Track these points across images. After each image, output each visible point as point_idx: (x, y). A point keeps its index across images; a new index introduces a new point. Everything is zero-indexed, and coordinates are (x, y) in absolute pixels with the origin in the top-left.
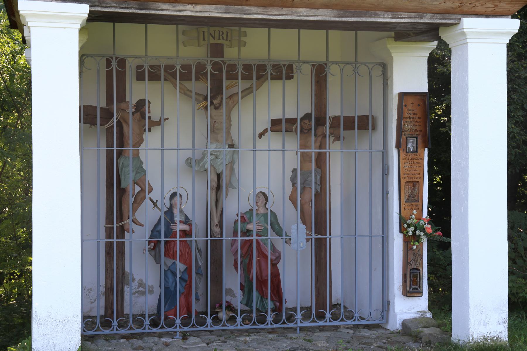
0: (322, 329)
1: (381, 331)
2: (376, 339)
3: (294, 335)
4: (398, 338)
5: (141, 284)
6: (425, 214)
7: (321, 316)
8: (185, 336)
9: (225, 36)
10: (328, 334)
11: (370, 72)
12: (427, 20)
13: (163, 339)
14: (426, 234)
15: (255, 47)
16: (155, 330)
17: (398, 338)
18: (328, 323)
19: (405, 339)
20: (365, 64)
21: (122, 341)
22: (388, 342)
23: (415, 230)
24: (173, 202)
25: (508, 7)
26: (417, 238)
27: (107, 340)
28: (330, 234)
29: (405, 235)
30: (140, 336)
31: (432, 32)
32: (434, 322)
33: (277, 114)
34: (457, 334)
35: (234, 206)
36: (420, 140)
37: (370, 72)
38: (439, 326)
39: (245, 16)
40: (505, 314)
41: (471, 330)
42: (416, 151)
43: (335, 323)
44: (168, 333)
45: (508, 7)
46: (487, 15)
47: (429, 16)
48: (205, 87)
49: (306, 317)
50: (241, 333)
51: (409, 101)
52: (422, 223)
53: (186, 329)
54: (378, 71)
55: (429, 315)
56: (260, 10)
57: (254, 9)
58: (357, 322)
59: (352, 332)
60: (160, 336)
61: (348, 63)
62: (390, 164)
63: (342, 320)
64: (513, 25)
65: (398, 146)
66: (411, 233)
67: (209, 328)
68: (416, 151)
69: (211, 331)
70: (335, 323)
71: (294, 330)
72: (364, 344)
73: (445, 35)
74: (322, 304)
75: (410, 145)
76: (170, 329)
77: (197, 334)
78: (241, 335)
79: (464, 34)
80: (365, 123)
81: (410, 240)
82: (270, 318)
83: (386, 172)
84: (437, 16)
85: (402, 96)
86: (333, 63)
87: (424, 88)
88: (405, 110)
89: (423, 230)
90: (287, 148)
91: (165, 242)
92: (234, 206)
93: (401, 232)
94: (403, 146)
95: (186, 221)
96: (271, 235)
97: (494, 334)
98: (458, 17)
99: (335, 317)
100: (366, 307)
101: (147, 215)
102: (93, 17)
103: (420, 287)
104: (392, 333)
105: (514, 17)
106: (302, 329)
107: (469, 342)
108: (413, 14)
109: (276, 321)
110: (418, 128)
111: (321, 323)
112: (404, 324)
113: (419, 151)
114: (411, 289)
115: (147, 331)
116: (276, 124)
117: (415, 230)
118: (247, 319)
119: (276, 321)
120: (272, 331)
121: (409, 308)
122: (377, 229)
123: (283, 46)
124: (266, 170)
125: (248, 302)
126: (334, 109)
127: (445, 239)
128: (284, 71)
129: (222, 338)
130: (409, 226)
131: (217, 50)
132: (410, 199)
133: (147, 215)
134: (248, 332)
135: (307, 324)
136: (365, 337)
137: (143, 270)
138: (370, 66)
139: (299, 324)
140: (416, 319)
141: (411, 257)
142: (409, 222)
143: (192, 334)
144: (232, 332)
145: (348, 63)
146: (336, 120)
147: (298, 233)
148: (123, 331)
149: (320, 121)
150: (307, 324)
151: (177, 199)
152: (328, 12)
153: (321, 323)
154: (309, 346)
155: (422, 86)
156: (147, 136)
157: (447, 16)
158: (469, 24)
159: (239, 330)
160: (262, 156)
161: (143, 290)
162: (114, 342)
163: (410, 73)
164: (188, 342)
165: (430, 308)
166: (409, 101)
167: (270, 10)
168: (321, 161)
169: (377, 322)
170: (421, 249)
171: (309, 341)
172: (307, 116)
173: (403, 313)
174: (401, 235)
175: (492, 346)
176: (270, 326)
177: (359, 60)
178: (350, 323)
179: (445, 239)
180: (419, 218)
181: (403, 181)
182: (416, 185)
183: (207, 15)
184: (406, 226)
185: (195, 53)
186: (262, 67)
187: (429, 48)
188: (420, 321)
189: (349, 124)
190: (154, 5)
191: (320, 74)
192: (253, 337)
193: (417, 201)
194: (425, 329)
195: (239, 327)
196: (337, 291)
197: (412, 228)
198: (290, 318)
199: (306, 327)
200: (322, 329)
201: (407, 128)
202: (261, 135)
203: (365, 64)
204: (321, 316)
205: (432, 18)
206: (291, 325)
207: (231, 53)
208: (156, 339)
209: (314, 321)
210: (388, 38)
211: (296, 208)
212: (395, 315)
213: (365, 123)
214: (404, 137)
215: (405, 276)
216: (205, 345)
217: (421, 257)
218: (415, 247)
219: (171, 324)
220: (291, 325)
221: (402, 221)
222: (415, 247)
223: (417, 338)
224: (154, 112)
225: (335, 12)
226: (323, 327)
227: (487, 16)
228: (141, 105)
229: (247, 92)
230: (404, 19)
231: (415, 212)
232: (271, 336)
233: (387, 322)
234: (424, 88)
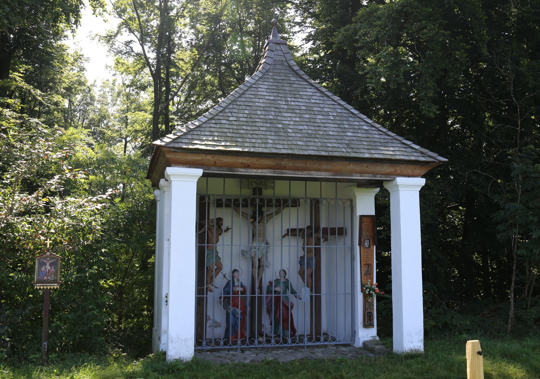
0: (318, 347)
1: (351, 348)
2: (350, 352)
3: (303, 350)
4: (362, 352)
5: (214, 321)
6: (375, 282)
7: (318, 340)
8: (243, 351)
9: (263, 183)
10: (322, 349)
11: (344, 204)
12: (378, 178)
13: (231, 352)
14: (376, 293)
15: (281, 189)
16: (226, 347)
17: (362, 352)
18: (322, 343)
19: (366, 351)
20: (341, 200)
21: (208, 353)
22: (357, 354)
23: (370, 291)
24: (234, 275)
25: (419, 172)
26: (370, 295)
27: (199, 353)
28: (311, 297)
29: (364, 294)
30: (218, 350)
31: (379, 184)
32: (381, 342)
33: (293, 226)
34: (396, 348)
35: (269, 275)
36: (371, 241)
37: (344, 204)
38: (384, 344)
39: (284, 175)
40: (422, 337)
41: (405, 345)
42: (369, 247)
43: (326, 343)
44: (232, 349)
45: (419, 172)
46: (409, 176)
47: (379, 176)
48: (249, 211)
49: (310, 340)
50: (273, 349)
51: (365, 220)
52: (373, 286)
53: (243, 346)
54: (348, 203)
55: (377, 338)
56: (291, 172)
57: (288, 171)
58: (338, 343)
59: (335, 348)
60: (229, 350)
61: (332, 199)
62: (355, 254)
63: (330, 342)
64: (422, 182)
65: (360, 244)
66: (367, 293)
67: (256, 346)
68: (369, 247)
69: (256, 348)
70: (326, 343)
71: (303, 347)
72: (343, 354)
73: (386, 186)
74: (316, 332)
75: (366, 244)
76: (235, 347)
77: (249, 349)
78: (273, 350)
79: (397, 186)
80: (341, 232)
81: (367, 296)
82: (290, 340)
83: (353, 258)
84: (383, 176)
85: (361, 217)
86: (324, 199)
87: (373, 212)
88: (363, 224)
89: (374, 290)
90: (291, 244)
91: (228, 298)
92: (269, 275)
93: (362, 292)
94: (362, 244)
95: (242, 286)
96: (289, 294)
97: (416, 348)
98: (394, 176)
99: (326, 340)
100: (342, 336)
101: (220, 281)
102: (204, 175)
103: (373, 322)
104: (358, 348)
105: (422, 177)
106: (308, 347)
107: (403, 352)
108: (371, 175)
109: (293, 342)
110: (370, 234)
111: (318, 343)
112: (364, 343)
113: (371, 247)
114: (367, 324)
115: (222, 347)
116: (293, 230)
117: (370, 291)
118: (277, 342)
119: (293, 342)
120: (290, 348)
121: (367, 335)
122: (349, 290)
123: (297, 190)
124: (283, 257)
125: (276, 332)
126: (323, 224)
127: (387, 296)
128: (295, 203)
129: (264, 352)
130: (366, 288)
131: (258, 191)
132: (366, 273)
133: (220, 281)
134: (278, 348)
135: (310, 344)
136: (343, 351)
137: (216, 313)
138: (344, 201)
139: (306, 344)
140: (370, 341)
141: (367, 306)
142: (366, 286)
143: (246, 349)
144: (268, 348)
145: (332, 199)
146: (325, 230)
147: (305, 293)
148: (209, 348)
149: (317, 229)
150: (310, 344)
151: (236, 274)
152: (327, 173)
153: (318, 343)
154: (313, 356)
155: (372, 212)
156: (220, 238)
157: (388, 176)
158: (400, 180)
159: (272, 348)
160: (285, 250)
161: (217, 325)
162: (203, 353)
163: (365, 205)
164: (245, 354)
165: (378, 334)
166: (365, 220)
167: (297, 172)
168: (318, 252)
169: (348, 343)
170: (373, 301)
171: (312, 353)
172: (309, 228)
173: (363, 337)
174: (362, 294)
175: (416, 354)
176: (290, 345)
177: (338, 197)
178: (334, 343)
179: (387, 296)
180: (372, 284)
181: (362, 264)
182: (370, 265)
183: (263, 174)
184: (365, 288)
185: (247, 192)
186: (286, 201)
187: (375, 192)
188: (372, 342)
189: (333, 231)
190: (236, 169)
191: (315, 204)
192: (281, 351)
193: (370, 275)
194: (376, 346)
195: (273, 345)
196: (324, 327)
197: (368, 290)
198: (301, 341)
199: (309, 346)
200: (318, 347)
201: (364, 234)
202: (284, 237)
203: (341, 200)
204: (318, 340)
205: (381, 177)
206: (301, 344)
207: (267, 193)
208: (227, 352)
209: (314, 342)
210: (354, 186)
211: (303, 279)
212: (359, 339)
213: (341, 232)
214: (363, 239)
215: (364, 316)
216: (255, 355)
217: (373, 306)
218: (370, 300)
219: (235, 343)
220: (301, 344)
221: (362, 286)
222: (370, 300)
223: (372, 351)
224: (226, 223)
225: (331, 173)
226: (318, 345)
227: (409, 176)
228: (219, 221)
229: (277, 213)
230: (366, 177)
231: (370, 280)
232: (290, 351)
233: (354, 343)
234: (373, 212)
